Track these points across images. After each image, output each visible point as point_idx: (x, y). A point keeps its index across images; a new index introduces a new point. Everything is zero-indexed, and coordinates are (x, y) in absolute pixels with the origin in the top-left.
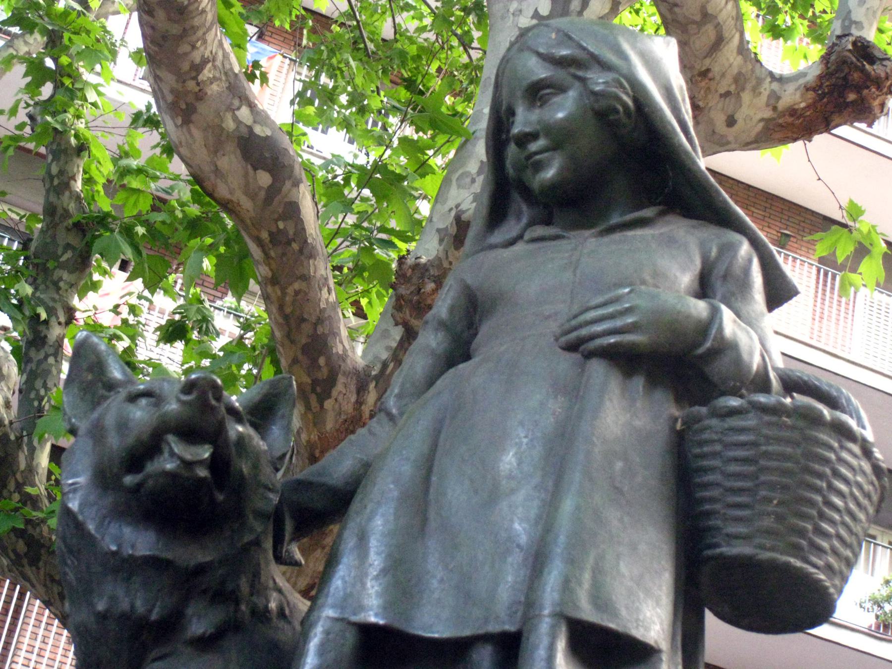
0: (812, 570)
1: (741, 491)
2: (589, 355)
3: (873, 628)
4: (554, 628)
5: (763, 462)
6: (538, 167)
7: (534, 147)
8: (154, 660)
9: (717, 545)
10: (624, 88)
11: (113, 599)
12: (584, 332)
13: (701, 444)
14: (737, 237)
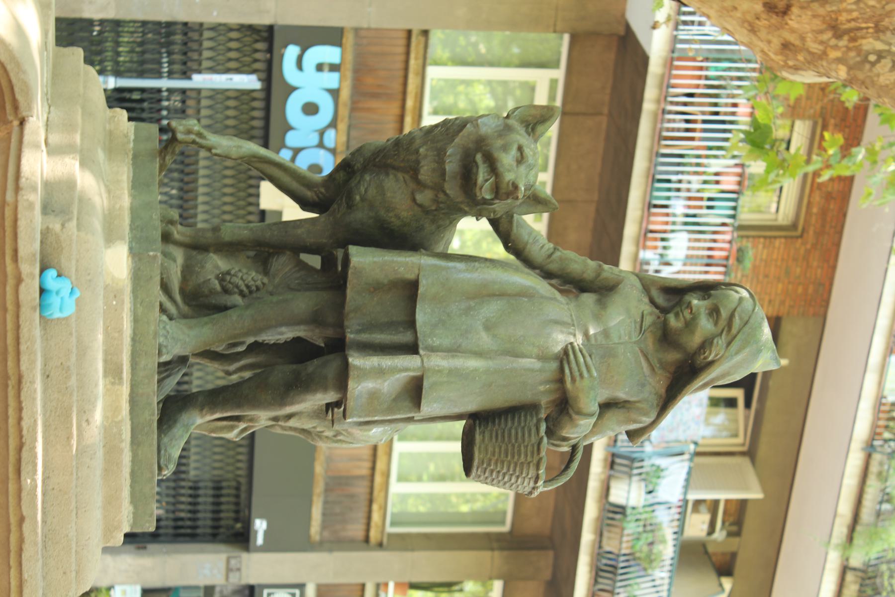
5: (516, 445)
6: (677, 315)
9: (480, 427)
11: (426, 156)
13: (525, 416)
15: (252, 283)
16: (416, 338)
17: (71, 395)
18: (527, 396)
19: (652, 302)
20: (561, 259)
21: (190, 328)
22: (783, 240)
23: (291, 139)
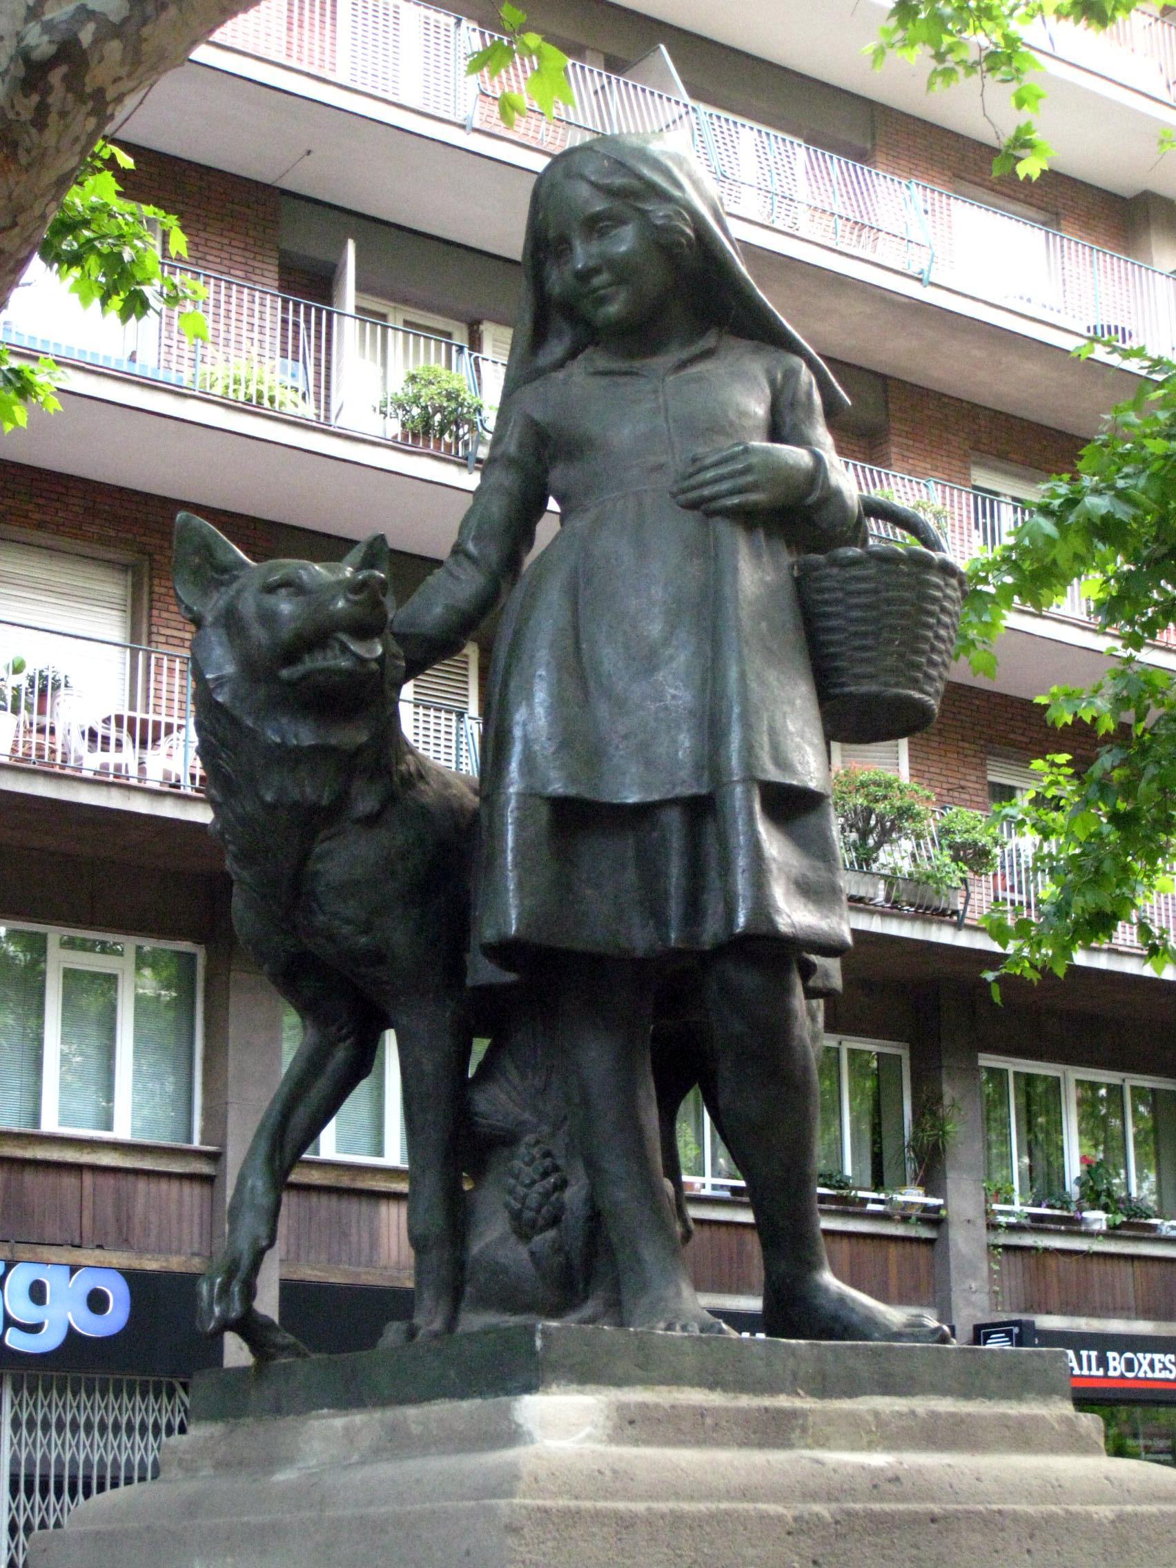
0: (927, 698)
1: (865, 635)
2: (710, 514)
3: (399, 439)
4: (748, 792)
6: (603, 301)
7: (597, 281)
8: (322, 841)
9: (843, 685)
10: (684, 219)
12: (706, 492)
13: (821, 591)
16: (675, 801)
17: (849, 1514)
19: (560, 365)
22: (156, 581)
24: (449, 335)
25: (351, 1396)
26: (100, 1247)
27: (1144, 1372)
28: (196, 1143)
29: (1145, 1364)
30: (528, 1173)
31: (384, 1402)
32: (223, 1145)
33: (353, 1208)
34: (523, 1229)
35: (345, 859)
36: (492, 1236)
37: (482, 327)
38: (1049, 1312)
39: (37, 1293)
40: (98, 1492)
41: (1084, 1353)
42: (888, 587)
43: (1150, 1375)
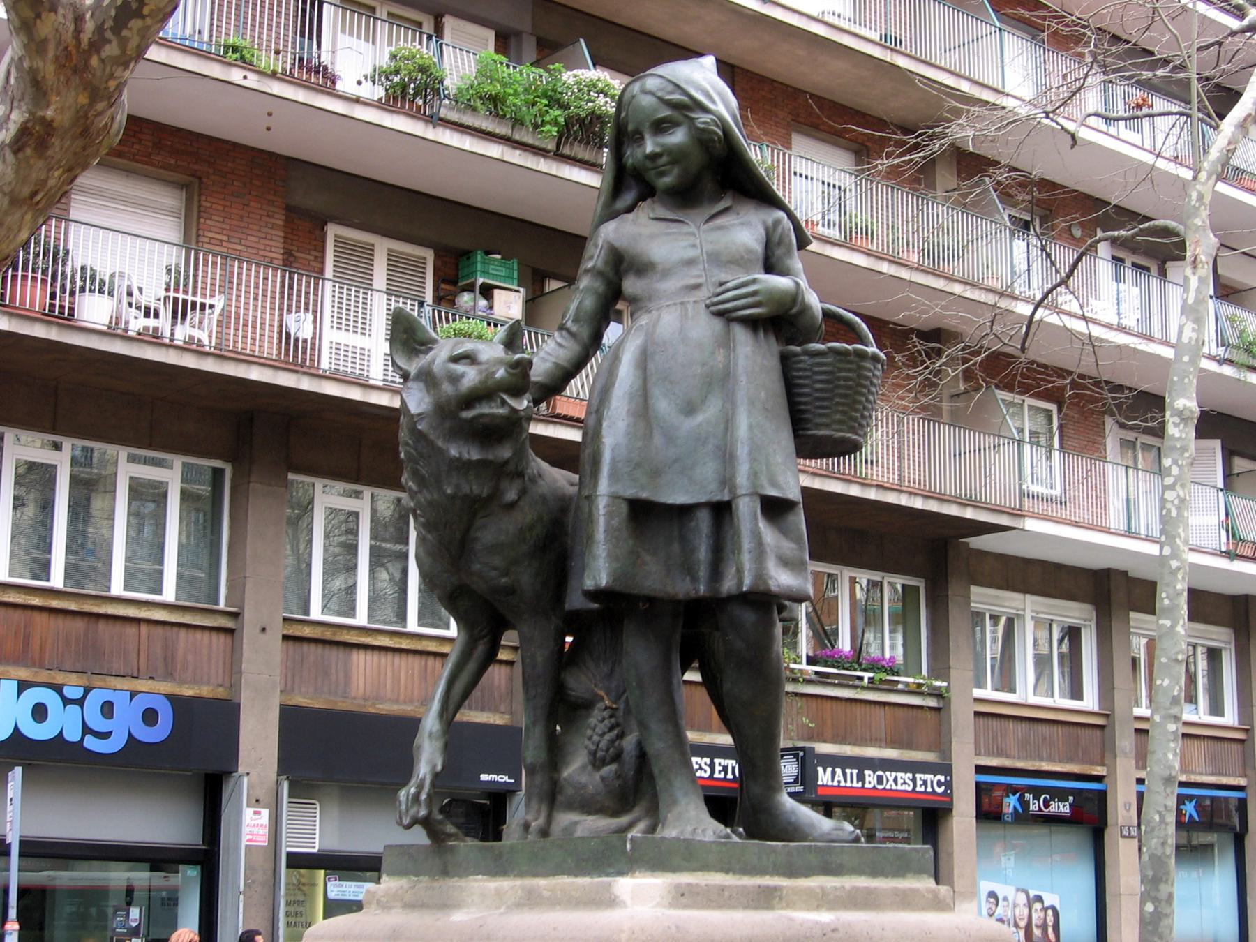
14: (781, 214)
15: (606, 722)
18: (773, 363)
19: (630, 210)
20: (576, 320)
21: (675, 802)
23: (73, 735)
24: (420, 25)
25: (500, 868)
26: (152, 678)
27: (890, 785)
28: (222, 605)
29: (891, 780)
30: (601, 728)
31: (521, 875)
32: (242, 608)
33: (334, 654)
34: (597, 762)
35: (494, 532)
36: (576, 769)
37: (444, 20)
38: (825, 741)
39: (107, 709)
40: (325, 917)
41: (848, 771)
42: (840, 370)
43: (894, 787)
